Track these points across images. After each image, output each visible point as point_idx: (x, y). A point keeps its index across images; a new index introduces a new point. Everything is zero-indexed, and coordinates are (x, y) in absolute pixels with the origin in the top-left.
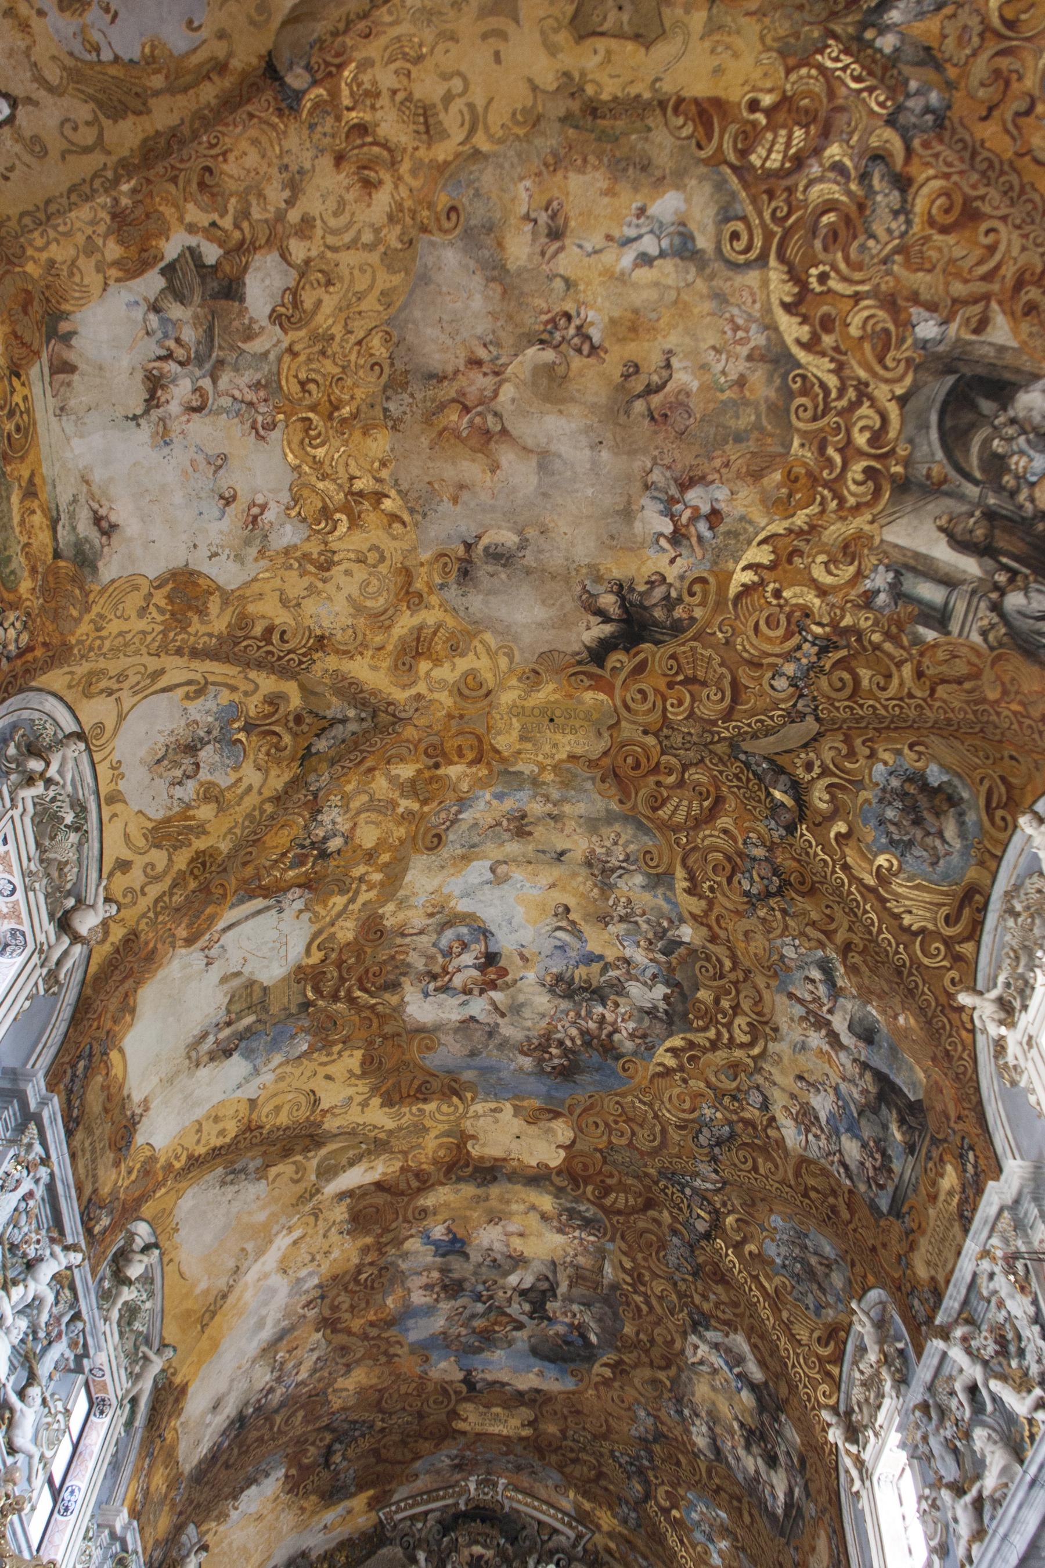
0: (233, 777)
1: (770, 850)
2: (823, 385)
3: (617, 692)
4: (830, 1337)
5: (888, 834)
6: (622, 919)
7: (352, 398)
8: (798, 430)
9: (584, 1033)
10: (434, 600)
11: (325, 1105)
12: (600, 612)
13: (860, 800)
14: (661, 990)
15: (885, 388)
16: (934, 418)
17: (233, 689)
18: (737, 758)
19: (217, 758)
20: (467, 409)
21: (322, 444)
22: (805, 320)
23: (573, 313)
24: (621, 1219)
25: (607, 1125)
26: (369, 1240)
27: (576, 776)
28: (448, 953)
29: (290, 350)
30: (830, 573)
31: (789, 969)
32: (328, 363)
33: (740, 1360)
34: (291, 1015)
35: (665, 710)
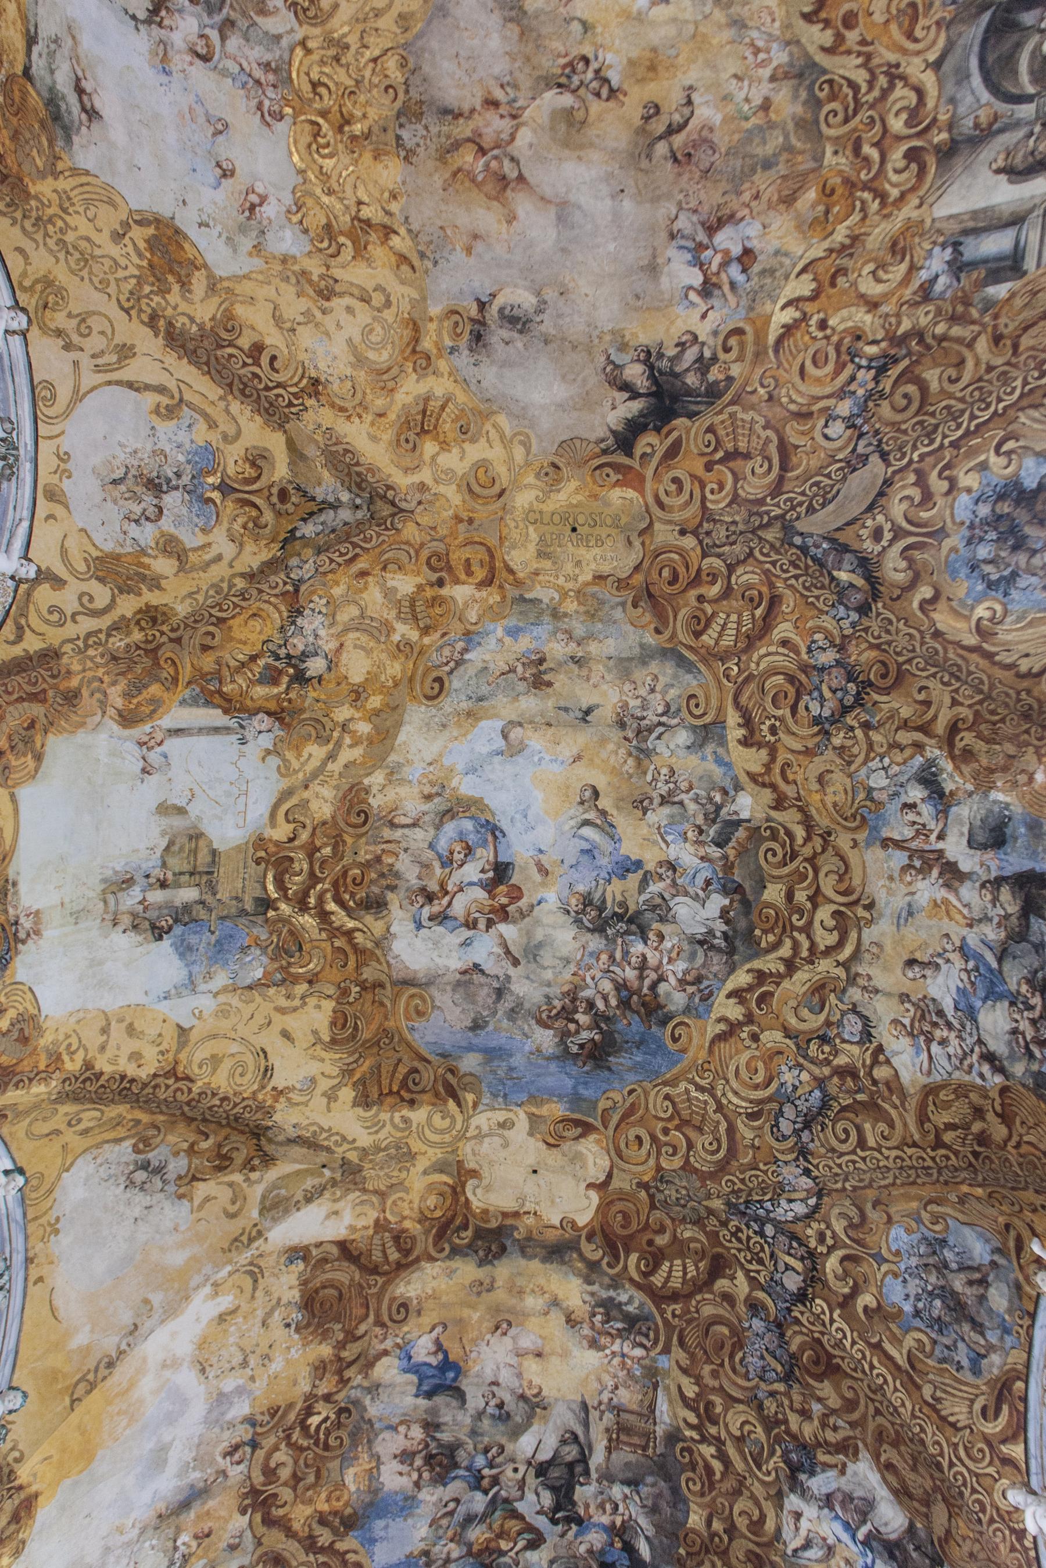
0: (200, 540)
1: (841, 648)
2: (852, 84)
3: (649, 485)
4: (999, 1400)
5: (984, 577)
6: (664, 801)
7: (364, 116)
8: (829, 138)
9: (620, 986)
10: (442, 365)
11: (279, 1080)
12: (626, 387)
13: (944, 551)
14: (717, 902)
15: (917, 61)
16: (974, 63)
17: (212, 425)
18: (792, 545)
19: (185, 511)
20: (482, 151)
21: (331, 156)
22: (827, 23)
23: (591, 56)
24: (678, 1308)
25: (654, 1138)
26: (326, 1350)
27: (602, 603)
28: (447, 862)
29: (303, 43)
30: (879, 281)
31: (880, 804)
32: (342, 71)
33: (865, 1509)
34: (243, 913)
35: (704, 499)
